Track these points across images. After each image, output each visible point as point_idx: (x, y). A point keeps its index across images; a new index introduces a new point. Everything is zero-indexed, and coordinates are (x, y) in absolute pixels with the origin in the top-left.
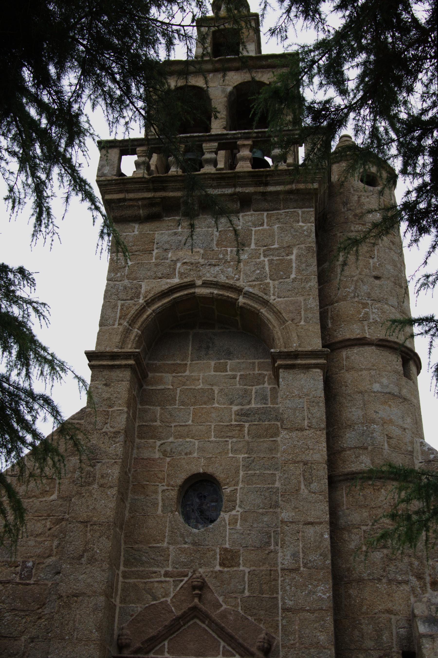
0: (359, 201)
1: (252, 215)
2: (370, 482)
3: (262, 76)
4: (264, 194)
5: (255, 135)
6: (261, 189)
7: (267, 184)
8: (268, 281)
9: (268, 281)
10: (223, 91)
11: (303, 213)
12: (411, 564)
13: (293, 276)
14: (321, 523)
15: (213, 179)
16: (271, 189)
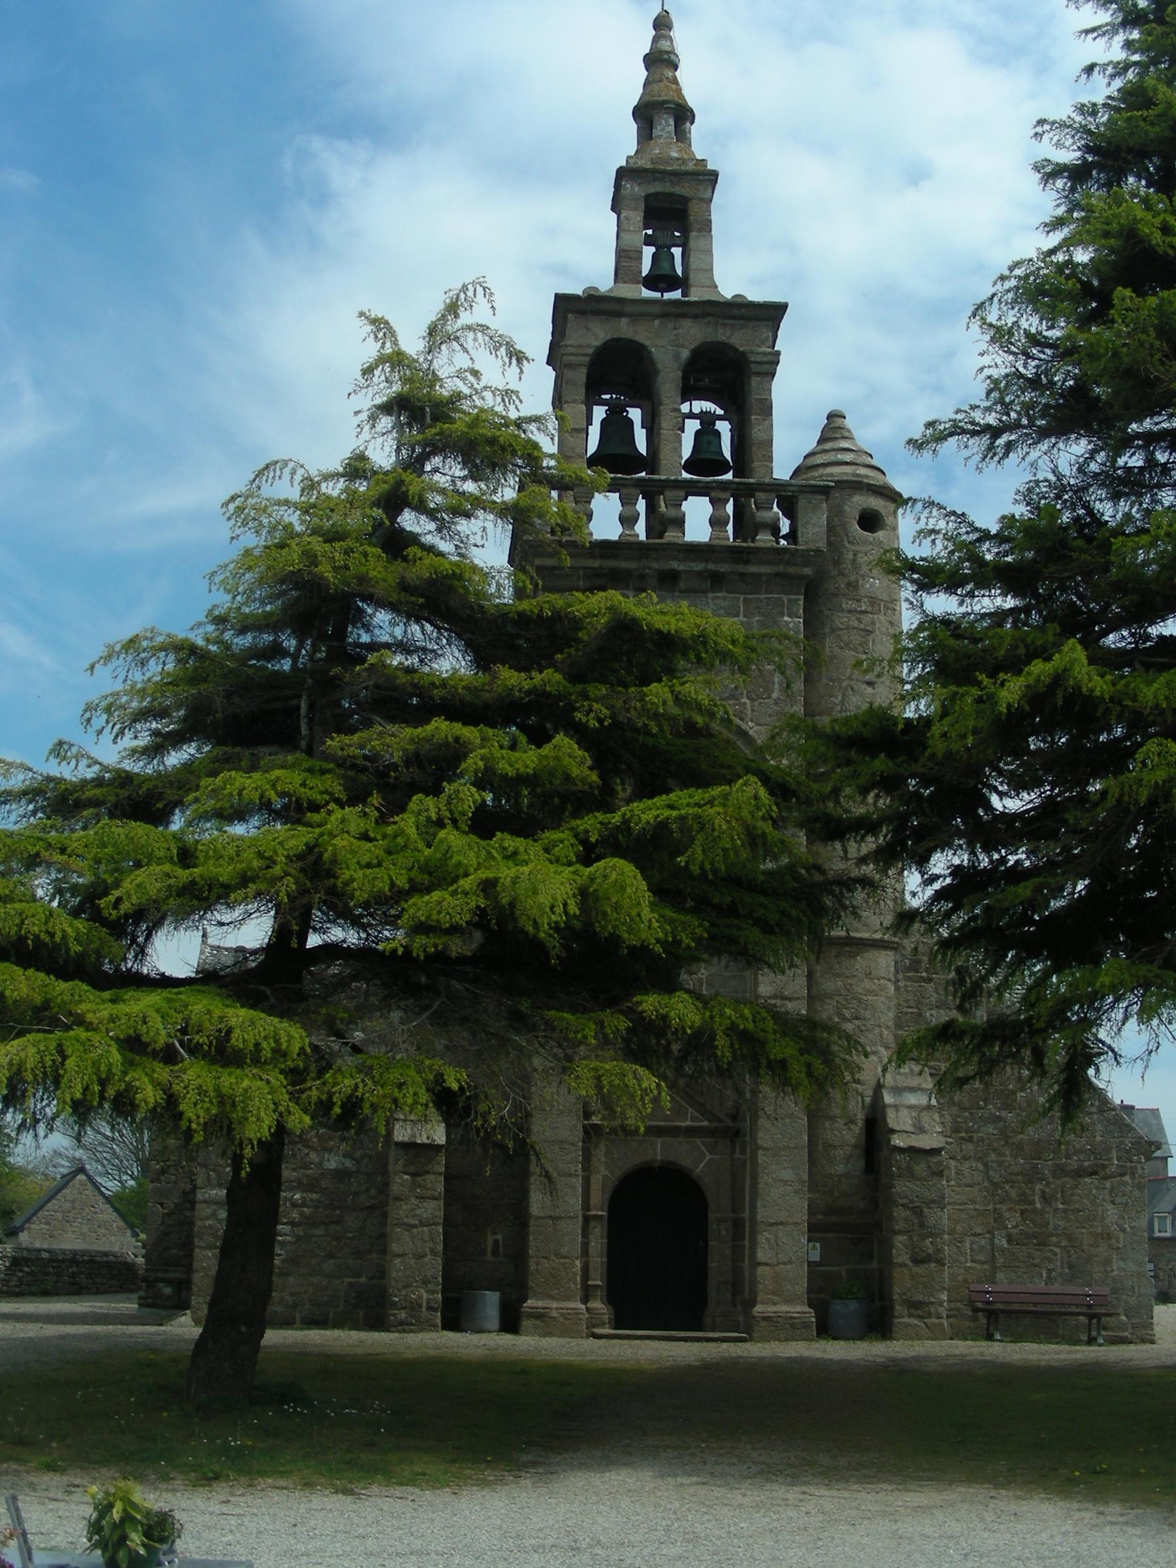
0: (854, 560)
1: (724, 598)
2: (847, 949)
3: (732, 334)
4: (742, 575)
5: (734, 486)
6: (740, 568)
7: (747, 562)
8: (744, 700)
9: (744, 700)
10: (677, 357)
11: (790, 601)
12: (881, 1035)
13: (775, 695)
14: (799, 998)
15: (679, 551)
16: (753, 569)
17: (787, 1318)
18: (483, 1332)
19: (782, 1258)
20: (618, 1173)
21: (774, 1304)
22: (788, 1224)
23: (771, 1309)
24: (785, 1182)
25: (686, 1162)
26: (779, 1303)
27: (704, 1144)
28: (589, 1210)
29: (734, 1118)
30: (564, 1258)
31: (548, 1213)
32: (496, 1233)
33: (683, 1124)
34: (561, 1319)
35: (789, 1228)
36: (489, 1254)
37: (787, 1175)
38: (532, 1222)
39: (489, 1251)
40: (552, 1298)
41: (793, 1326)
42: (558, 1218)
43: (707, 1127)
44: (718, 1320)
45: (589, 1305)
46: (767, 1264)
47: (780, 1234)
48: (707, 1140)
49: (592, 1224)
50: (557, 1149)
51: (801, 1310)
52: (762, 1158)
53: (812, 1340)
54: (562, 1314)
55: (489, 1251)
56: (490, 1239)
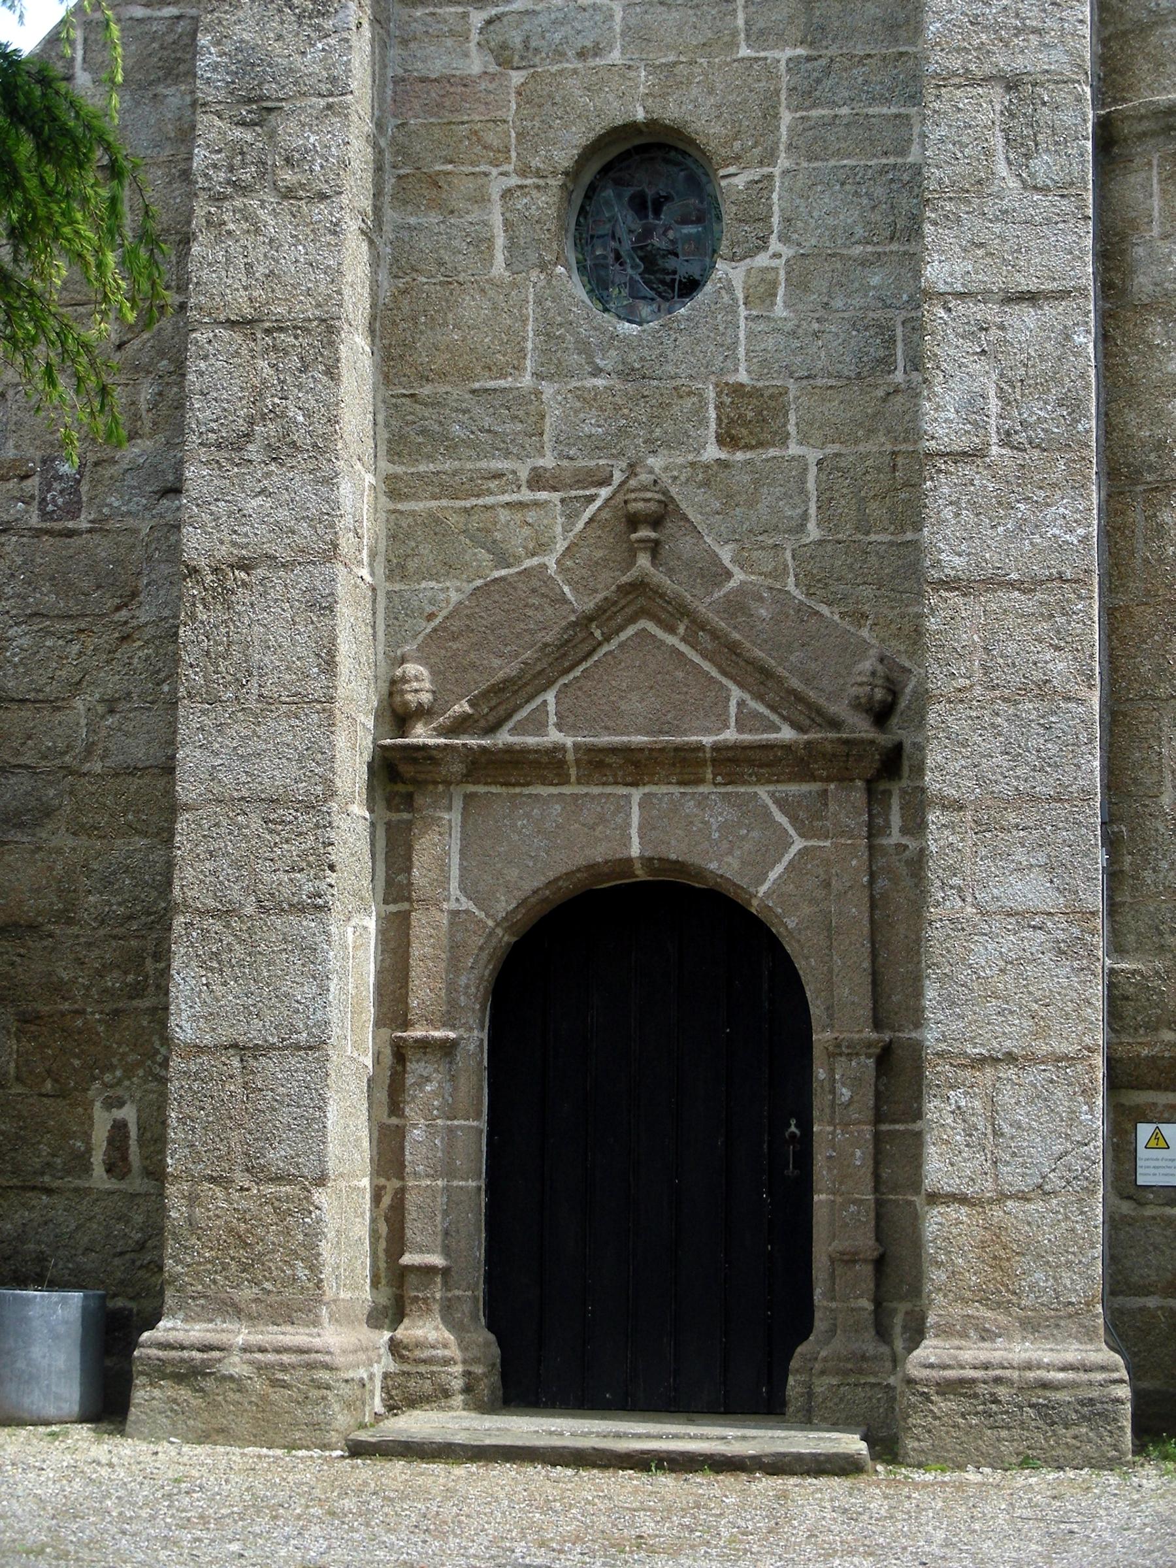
17: (1026, 1387)
18: (21, 1423)
19: (1013, 1177)
20: (504, 905)
21: (986, 1335)
22: (1032, 1059)
23: (973, 1352)
24: (1022, 917)
25: (723, 864)
26: (1003, 1332)
27: (781, 804)
28: (406, 1025)
29: (882, 714)
30: (277, 1179)
31: (226, 1034)
32: (121, 1104)
33: (707, 740)
34: (259, 1385)
35: (1035, 1075)
36: (99, 1170)
37: (1031, 890)
38: (176, 1063)
39: (98, 1159)
40: (237, 1311)
41: (1045, 1412)
42: (257, 1051)
43: (787, 748)
44: (822, 1385)
45: (400, 1333)
46: (963, 1200)
47: (1006, 1096)
48: (793, 788)
49: (416, 1067)
50: (256, 823)
51: (1084, 1358)
52: (941, 835)
53: (1111, 1464)
54: (260, 1368)
55: (98, 1159)
56: (102, 1123)
